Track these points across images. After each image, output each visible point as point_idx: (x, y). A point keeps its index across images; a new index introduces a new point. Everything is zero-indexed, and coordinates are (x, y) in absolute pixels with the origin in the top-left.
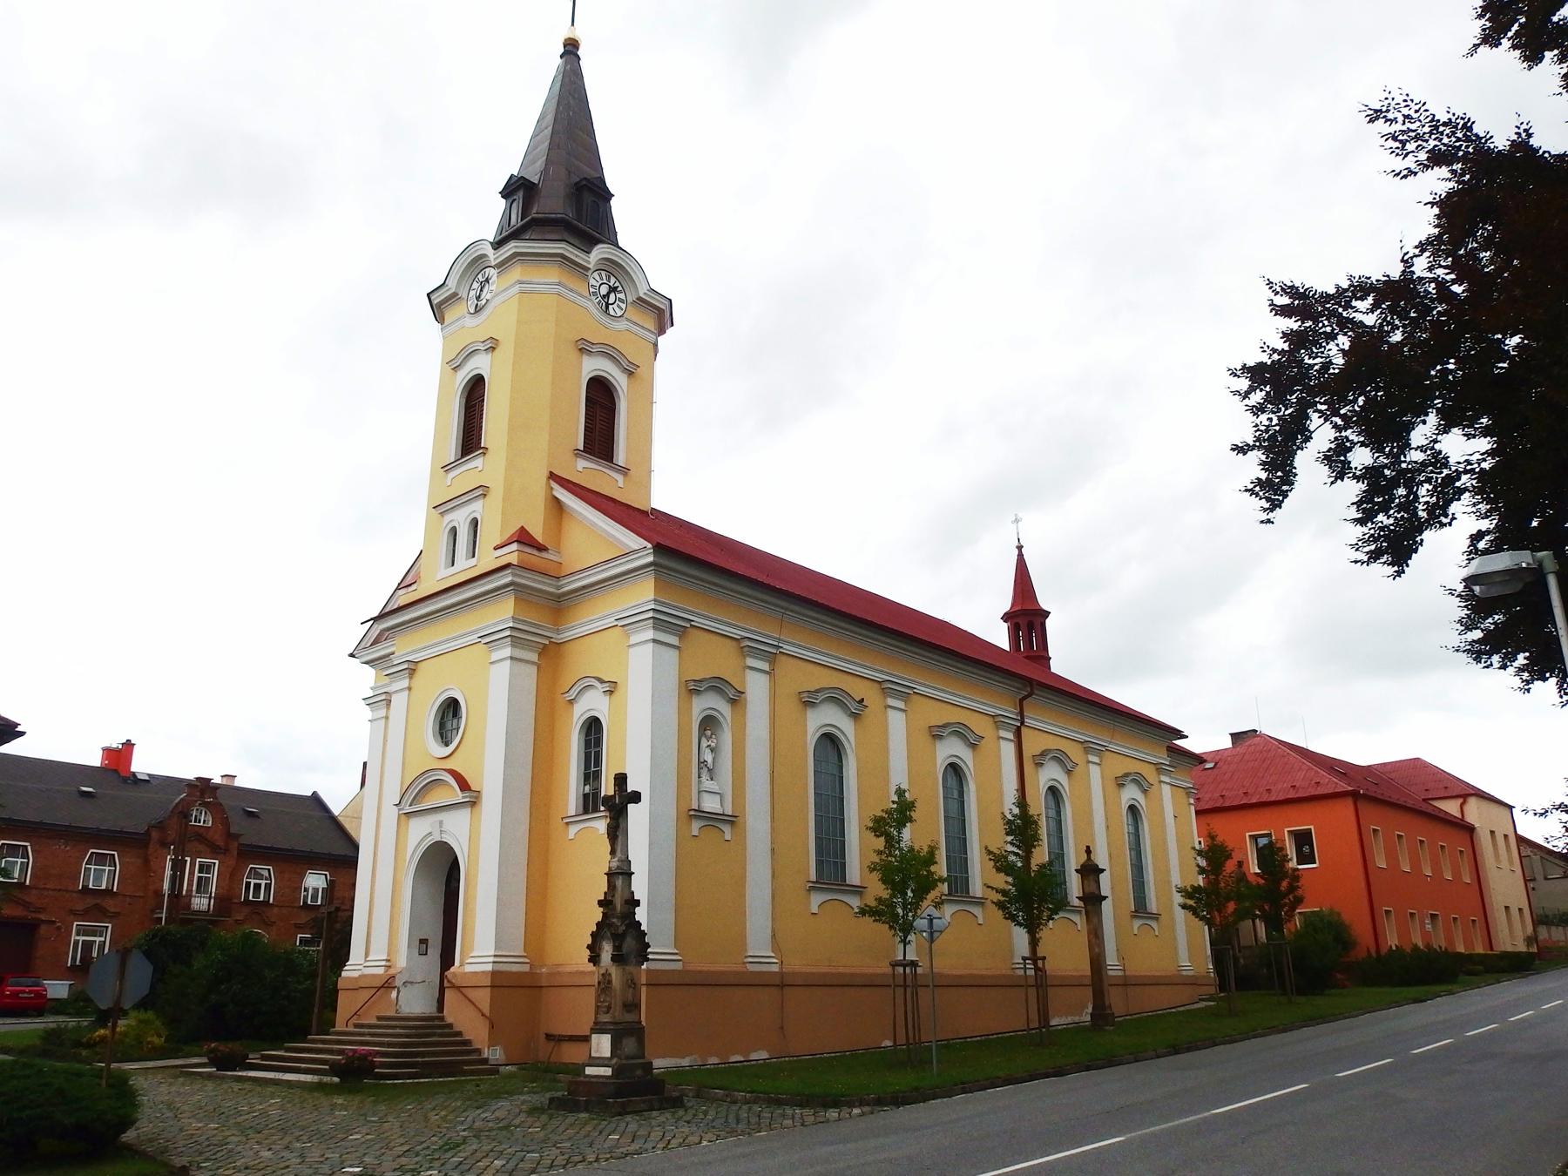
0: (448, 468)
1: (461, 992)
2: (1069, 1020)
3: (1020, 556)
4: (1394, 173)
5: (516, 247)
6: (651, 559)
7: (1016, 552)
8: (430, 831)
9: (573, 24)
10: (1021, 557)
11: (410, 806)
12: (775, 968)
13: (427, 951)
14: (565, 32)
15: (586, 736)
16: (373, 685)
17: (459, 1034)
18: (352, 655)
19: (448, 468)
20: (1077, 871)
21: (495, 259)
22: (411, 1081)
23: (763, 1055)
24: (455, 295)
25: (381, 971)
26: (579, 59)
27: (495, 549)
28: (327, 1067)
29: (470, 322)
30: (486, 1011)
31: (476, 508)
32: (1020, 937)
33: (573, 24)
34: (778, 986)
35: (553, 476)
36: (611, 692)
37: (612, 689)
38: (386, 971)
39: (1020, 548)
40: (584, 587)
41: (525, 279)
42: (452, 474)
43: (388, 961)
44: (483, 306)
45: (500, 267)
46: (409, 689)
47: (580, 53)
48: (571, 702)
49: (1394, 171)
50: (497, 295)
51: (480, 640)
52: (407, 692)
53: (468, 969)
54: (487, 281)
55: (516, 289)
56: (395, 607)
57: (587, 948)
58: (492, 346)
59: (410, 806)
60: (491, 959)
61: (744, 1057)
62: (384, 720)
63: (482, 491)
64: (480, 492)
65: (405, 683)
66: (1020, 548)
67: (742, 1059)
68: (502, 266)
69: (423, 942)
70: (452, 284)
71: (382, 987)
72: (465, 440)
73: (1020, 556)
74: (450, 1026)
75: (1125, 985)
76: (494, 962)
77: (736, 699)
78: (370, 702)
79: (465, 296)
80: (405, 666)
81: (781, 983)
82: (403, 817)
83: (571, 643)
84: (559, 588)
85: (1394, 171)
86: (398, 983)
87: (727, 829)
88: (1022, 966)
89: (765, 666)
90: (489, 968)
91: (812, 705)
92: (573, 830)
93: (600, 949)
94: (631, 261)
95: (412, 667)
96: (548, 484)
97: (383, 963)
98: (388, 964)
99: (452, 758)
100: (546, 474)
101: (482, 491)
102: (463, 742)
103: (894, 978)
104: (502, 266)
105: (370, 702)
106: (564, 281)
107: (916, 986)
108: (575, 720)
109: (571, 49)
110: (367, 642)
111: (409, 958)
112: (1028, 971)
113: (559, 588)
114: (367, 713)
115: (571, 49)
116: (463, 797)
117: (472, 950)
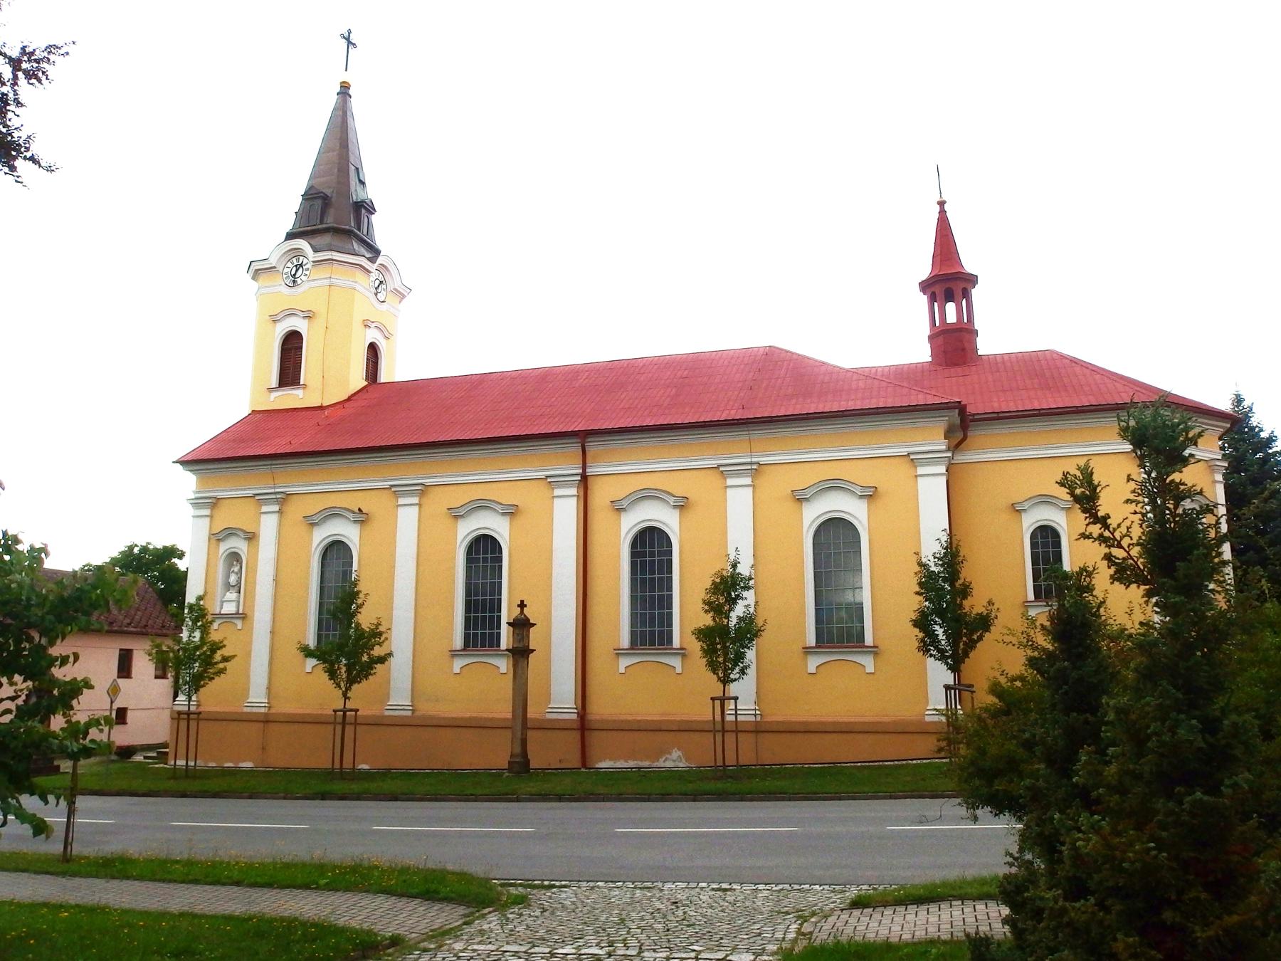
2: (631, 764)
3: (943, 213)
4: (19, 180)
7: (938, 208)
9: (346, 70)
10: (943, 213)
19: (270, 390)
20: (509, 624)
23: (249, 765)
32: (939, 674)
38: (197, 708)
39: (942, 204)
49: (16, 181)
57: (944, 686)
61: (234, 764)
66: (942, 204)
67: (233, 766)
73: (943, 213)
75: (757, 732)
77: (251, 537)
79: (281, 270)
81: (266, 720)
85: (16, 181)
87: (239, 624)
88: (734, 712)
89: (276, 508)
91: (313, 525)
103: (714, 724)
107: (724, 731)
109: (345, 90)
112: (738, 716)
115: (345, 90)
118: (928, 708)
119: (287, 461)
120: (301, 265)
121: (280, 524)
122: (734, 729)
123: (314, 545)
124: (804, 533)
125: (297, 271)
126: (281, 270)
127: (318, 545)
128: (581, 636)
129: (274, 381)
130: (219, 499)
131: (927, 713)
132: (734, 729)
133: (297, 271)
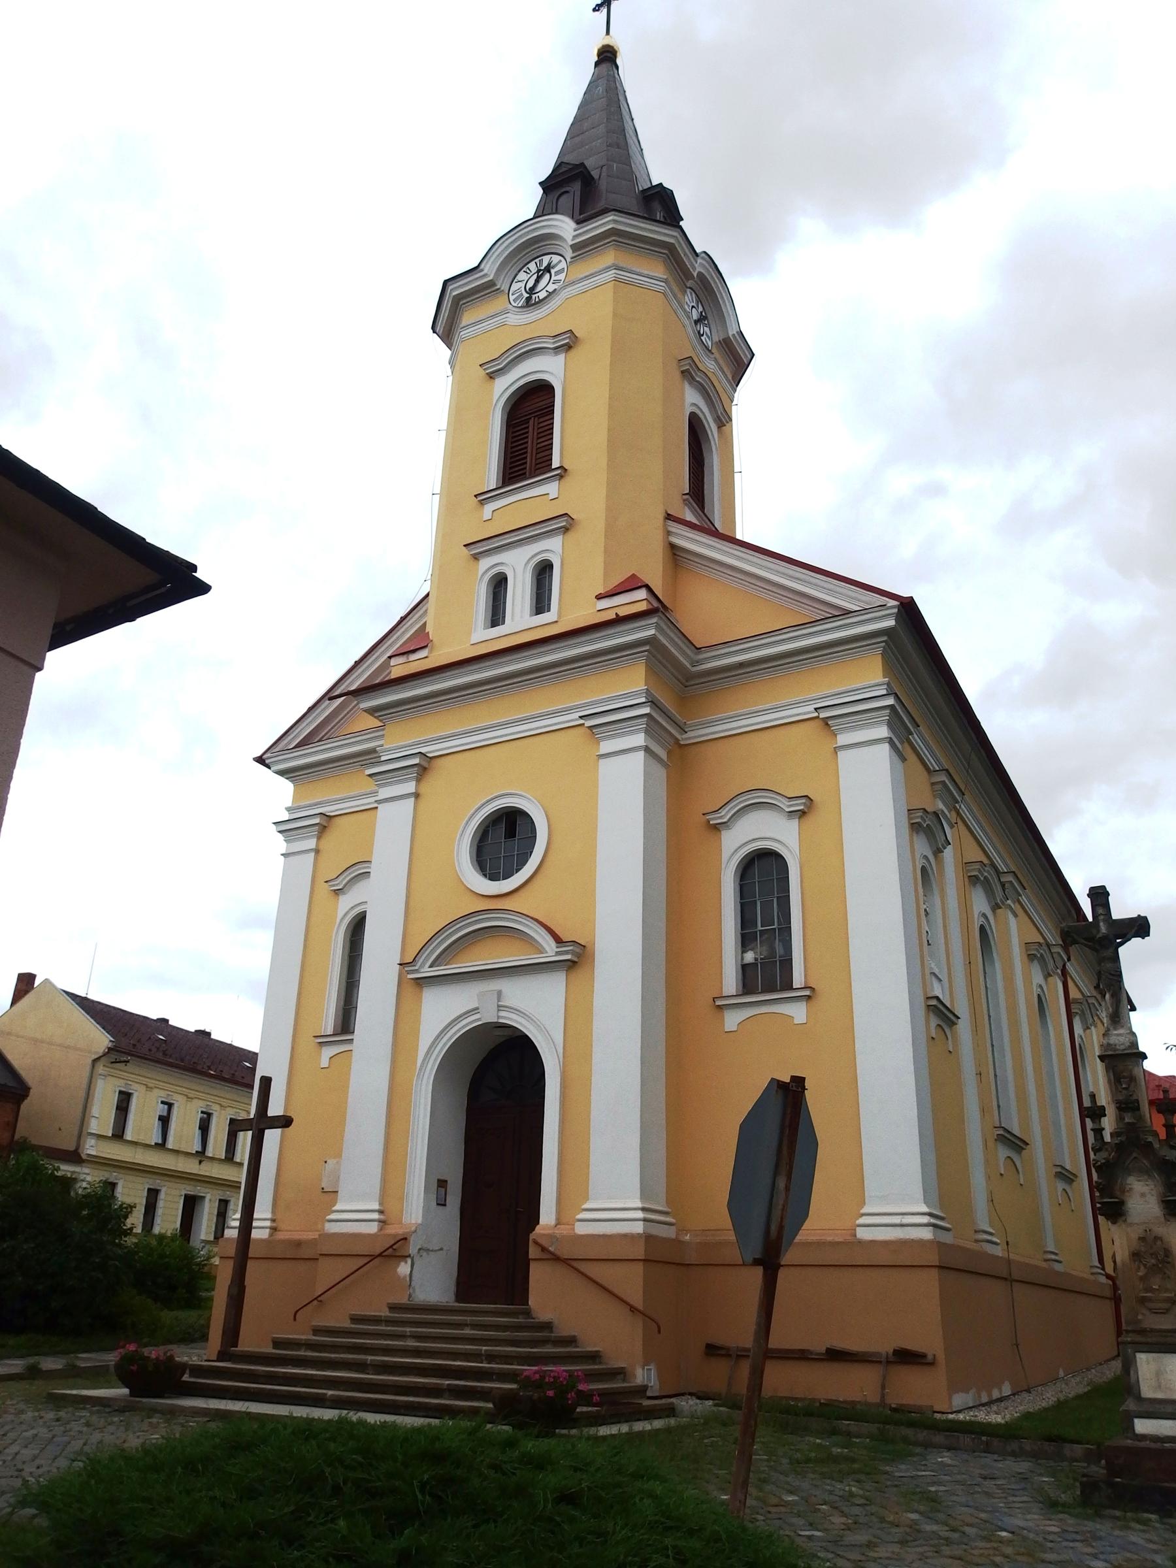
0: (483, 498)
1: (569, 1265)
5: (615, 221)
6: (891, 623)
8: (476, 1005)
9: (608, 32)
11: (430, 967)
12: (998, 1251)
13: (445, 1200)
14: (601, 40)
15: (741, 881)
16: (290, 804)
17: (572, 1341)
18: (260, 760)
19: (483, 498)
21: (575, 237)
22: (625, 1428)
24: (491, 284)
25: (373, 1228)
26: (617, 68)
27: (599, 597)
28: (490, 1405)
29: (514, 319)
30: (637, 1300)
31: (553, 548)
33: (608, 32)
34: (1006, 1279)
35: (669, 517)
36: (802, 814)
37: (804, 810)
38: (381, 1229)
40: (741, 665)
41: (621, 264)
42: (489, 508)
43: (381, 1212)
44: (541, 301)
45: (579, 249)
46: (417, 795)
47: (619, 61)
48: (716, 828)
50: (565, 287)
51: (581, 722)
52: (413, 799)
53: (581, 1229)
54: (548, 269)
55: (611, 274)
56: (353, 688)
58: (568, 344)
59: (430, 967)
60: (640, 1215)
62: (312, 854)
63: (564, 524)
64: (562, 523)
65: (410, 787)
68: (582, 249)
69: (442, 1184)
70: (490, 270)
71: (380, 1255)
72: (508, 462)
74: (548, 1326)
76: (645, 1220)
78: (287, 829)
79: (505, 287)
80: (416, 761)
82: (409, 990)
83: (710, 744)
84: (695, 663)
86: (413, 1250)
90: (639, 1228)
92: (732, 1020)
93: (1123, 1191)
94: (724, 289)
95: (425, 764)
96: (665, 526)
97: (376, 1216)
98: (382, 1217)
99: (516, 895)
100: (661, 516)
101: (564, 524)
102: (542, 870)
104: (582, 249)
105: (287, 829)
106: (670, 279)
108: (725, 855)
109: (607, 56)
110: (289, 743)
111: (426, 1210)
113: (695, 663)
114: (280, 844)
115: (607, 56)
116: (558, 953)
117: (586, 1198)
118: (863, 1211)
119: (434, 677)
120: (548, 269)
121: (316, 860)
122: (776, 1341)
123: (340, 914)
124: (723, 866)
125: (537, 281)
126: (505, 287)
127: (345, 915)
128: (1086, 1174)
129: (491, 478)
130: (431, 758)
131: (862, 1221)
132: (776, 1341)
133: (537, 281)
